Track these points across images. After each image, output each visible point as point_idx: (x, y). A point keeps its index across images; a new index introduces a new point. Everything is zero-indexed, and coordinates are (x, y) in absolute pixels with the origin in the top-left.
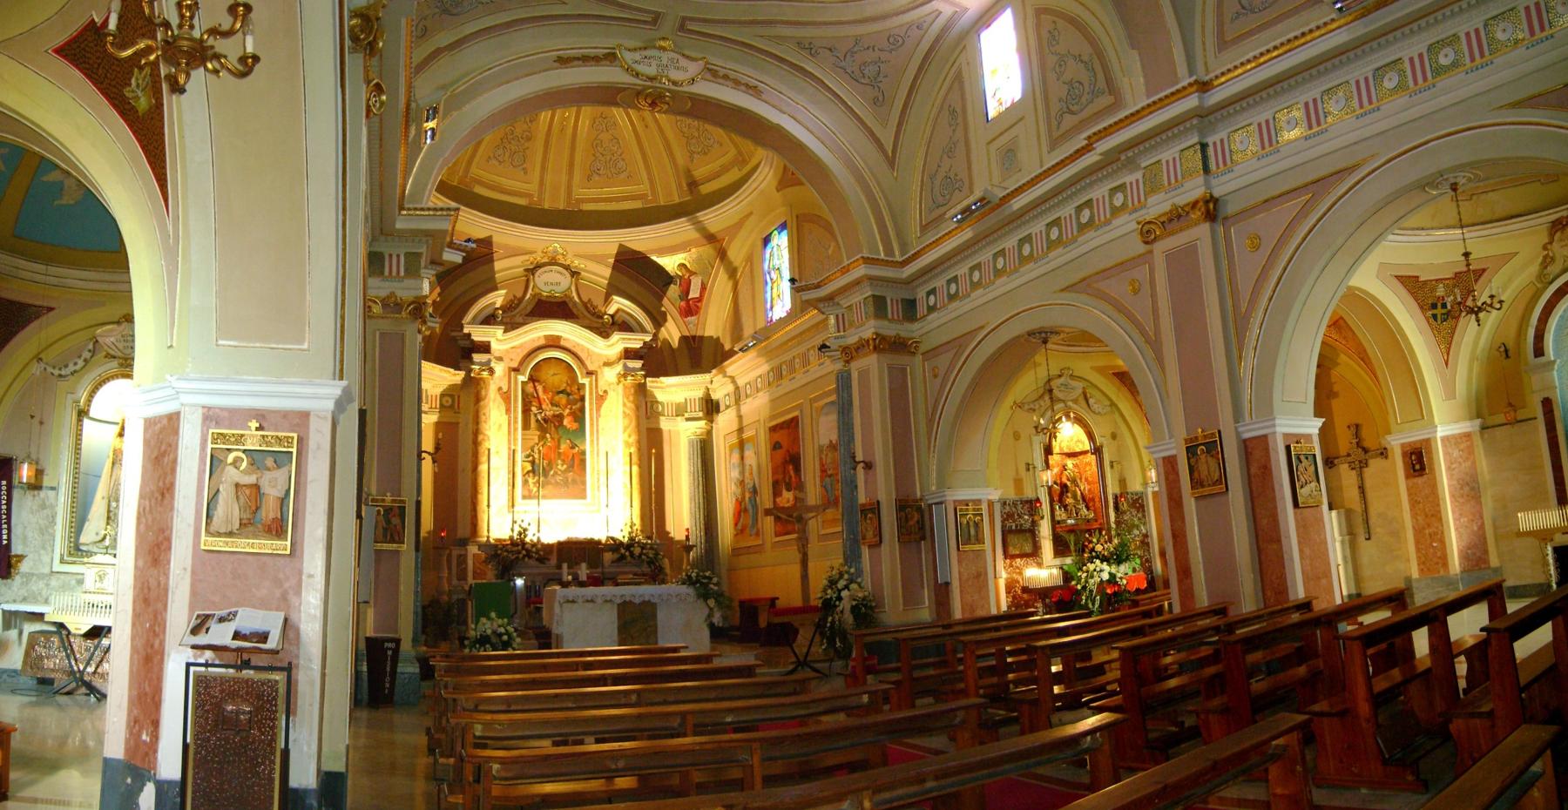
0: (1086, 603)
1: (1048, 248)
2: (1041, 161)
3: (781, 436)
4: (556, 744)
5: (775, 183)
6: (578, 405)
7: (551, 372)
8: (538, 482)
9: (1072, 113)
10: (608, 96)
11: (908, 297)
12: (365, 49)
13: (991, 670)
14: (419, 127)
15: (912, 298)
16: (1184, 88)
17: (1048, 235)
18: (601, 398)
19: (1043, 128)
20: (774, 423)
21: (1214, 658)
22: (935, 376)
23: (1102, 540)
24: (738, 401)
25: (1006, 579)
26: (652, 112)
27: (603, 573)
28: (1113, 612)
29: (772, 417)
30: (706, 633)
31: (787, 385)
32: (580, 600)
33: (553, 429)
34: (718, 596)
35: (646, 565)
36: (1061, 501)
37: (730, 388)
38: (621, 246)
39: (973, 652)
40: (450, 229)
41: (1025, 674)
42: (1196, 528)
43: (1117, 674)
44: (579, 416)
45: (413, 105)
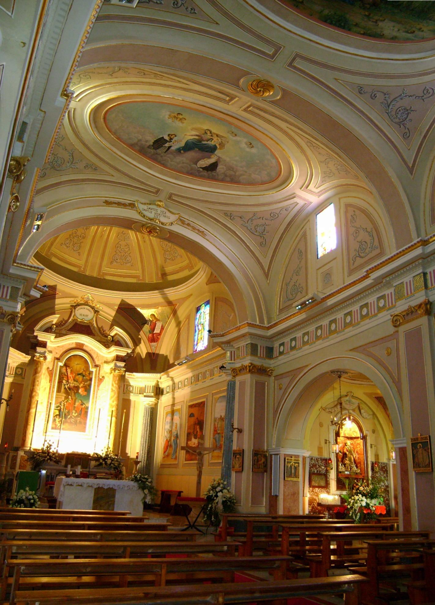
0: (352, 516)
1: (345, 327)
2: (344, 281)
3: (195, 411)
4: (52, 558)
5: (205, 281)
6: (88, 383)
7: (76, 363)
8: (61, 421)
9: (360, 257)
10: (128, 224)
11: (269, 346)
12: (15, 178)
13: (296, 543)
14: (32, 223)
15: (271, 346)
16: (415, 244)
17: (345, 320)
18: (101, 380)
19: (346, 264)
20: (192, 403)
21: (419, 559)
22: (280, 389)
23: (364, 485)
24: (173, 390)
25: (309, 498)
26: (149, 236)
27: (89, 471)
28: (366, 523)
29: (191, 400)
30: (141, 506)
31: (200, 385)
32: (75, 484)
33: (73, 394)
34: (151, 489)
35: (112, 469)
36: (342, 461)
37: (170, 383)
38: (122, 300)
39: (288, 532)
40: (37, 279)
41: (316, 547)
42: (415, 489)
43: (366, 556)
44: (88, 389)
45: (32, 210)
